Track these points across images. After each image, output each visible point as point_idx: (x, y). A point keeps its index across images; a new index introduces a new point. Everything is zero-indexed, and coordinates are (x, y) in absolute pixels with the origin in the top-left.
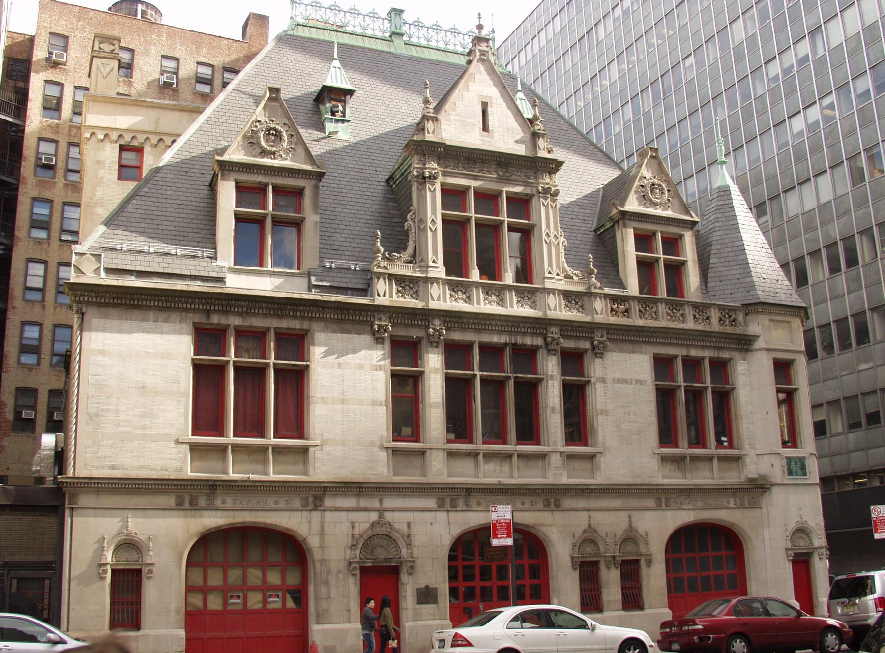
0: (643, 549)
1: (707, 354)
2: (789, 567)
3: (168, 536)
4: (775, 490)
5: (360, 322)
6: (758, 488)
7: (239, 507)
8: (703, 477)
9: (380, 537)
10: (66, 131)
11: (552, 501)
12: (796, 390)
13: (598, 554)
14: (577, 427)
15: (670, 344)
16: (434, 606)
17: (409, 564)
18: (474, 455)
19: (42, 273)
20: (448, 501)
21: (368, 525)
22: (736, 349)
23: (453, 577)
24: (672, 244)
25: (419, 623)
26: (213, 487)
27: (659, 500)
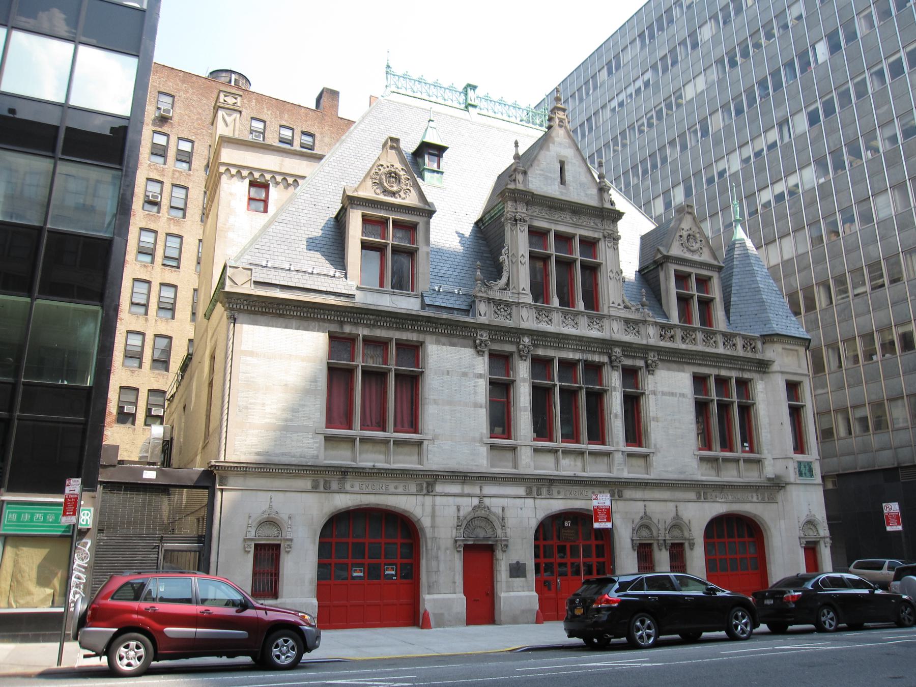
0: (686, 534)
1: (734, 374)
2: (801, 553)
3: (304, 514)
4: (789, 487)
5: (465, 337)
6: (776, 485)
7: (367, 491)
8: (730, 475)
9: (480, 518)
10: (170, 174)
11: (616, 491)
12: (803, 406)
13: (652, 537)
14: (635, 432)
15: (706, 365)
16: (523, 579)
17: (504, 543)
18: (555, 451)
19: (146, 291)
20: (535, 489)
21: (470, 509)
22: (756, 371)
23: (537, 556)
24: (703, 282)
25: (512, 594)
26: (344, 472)
27: (699, 494)
